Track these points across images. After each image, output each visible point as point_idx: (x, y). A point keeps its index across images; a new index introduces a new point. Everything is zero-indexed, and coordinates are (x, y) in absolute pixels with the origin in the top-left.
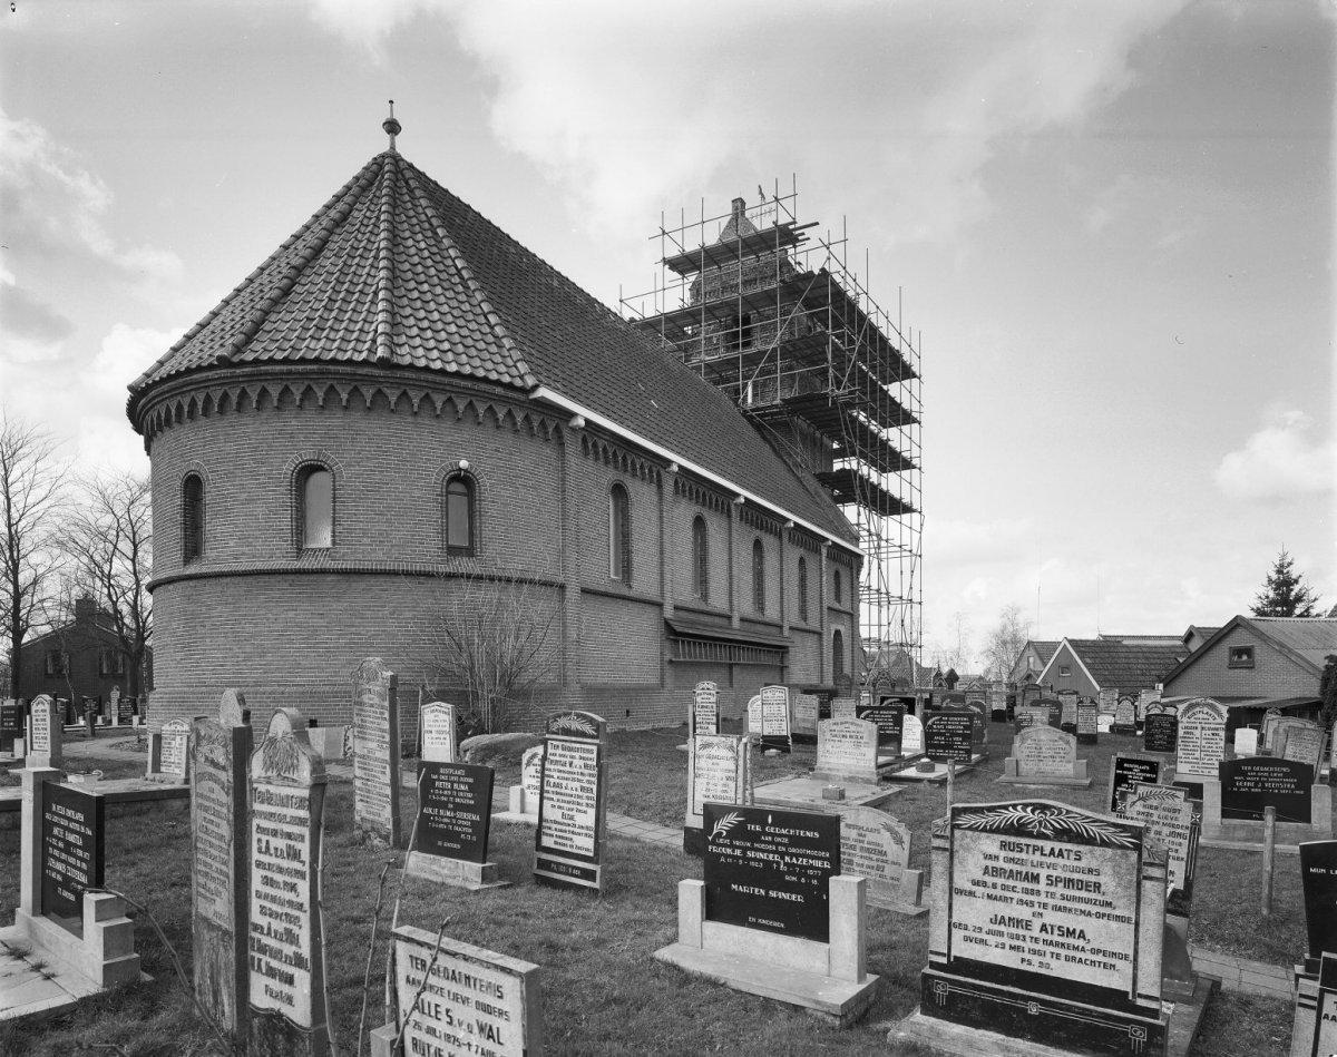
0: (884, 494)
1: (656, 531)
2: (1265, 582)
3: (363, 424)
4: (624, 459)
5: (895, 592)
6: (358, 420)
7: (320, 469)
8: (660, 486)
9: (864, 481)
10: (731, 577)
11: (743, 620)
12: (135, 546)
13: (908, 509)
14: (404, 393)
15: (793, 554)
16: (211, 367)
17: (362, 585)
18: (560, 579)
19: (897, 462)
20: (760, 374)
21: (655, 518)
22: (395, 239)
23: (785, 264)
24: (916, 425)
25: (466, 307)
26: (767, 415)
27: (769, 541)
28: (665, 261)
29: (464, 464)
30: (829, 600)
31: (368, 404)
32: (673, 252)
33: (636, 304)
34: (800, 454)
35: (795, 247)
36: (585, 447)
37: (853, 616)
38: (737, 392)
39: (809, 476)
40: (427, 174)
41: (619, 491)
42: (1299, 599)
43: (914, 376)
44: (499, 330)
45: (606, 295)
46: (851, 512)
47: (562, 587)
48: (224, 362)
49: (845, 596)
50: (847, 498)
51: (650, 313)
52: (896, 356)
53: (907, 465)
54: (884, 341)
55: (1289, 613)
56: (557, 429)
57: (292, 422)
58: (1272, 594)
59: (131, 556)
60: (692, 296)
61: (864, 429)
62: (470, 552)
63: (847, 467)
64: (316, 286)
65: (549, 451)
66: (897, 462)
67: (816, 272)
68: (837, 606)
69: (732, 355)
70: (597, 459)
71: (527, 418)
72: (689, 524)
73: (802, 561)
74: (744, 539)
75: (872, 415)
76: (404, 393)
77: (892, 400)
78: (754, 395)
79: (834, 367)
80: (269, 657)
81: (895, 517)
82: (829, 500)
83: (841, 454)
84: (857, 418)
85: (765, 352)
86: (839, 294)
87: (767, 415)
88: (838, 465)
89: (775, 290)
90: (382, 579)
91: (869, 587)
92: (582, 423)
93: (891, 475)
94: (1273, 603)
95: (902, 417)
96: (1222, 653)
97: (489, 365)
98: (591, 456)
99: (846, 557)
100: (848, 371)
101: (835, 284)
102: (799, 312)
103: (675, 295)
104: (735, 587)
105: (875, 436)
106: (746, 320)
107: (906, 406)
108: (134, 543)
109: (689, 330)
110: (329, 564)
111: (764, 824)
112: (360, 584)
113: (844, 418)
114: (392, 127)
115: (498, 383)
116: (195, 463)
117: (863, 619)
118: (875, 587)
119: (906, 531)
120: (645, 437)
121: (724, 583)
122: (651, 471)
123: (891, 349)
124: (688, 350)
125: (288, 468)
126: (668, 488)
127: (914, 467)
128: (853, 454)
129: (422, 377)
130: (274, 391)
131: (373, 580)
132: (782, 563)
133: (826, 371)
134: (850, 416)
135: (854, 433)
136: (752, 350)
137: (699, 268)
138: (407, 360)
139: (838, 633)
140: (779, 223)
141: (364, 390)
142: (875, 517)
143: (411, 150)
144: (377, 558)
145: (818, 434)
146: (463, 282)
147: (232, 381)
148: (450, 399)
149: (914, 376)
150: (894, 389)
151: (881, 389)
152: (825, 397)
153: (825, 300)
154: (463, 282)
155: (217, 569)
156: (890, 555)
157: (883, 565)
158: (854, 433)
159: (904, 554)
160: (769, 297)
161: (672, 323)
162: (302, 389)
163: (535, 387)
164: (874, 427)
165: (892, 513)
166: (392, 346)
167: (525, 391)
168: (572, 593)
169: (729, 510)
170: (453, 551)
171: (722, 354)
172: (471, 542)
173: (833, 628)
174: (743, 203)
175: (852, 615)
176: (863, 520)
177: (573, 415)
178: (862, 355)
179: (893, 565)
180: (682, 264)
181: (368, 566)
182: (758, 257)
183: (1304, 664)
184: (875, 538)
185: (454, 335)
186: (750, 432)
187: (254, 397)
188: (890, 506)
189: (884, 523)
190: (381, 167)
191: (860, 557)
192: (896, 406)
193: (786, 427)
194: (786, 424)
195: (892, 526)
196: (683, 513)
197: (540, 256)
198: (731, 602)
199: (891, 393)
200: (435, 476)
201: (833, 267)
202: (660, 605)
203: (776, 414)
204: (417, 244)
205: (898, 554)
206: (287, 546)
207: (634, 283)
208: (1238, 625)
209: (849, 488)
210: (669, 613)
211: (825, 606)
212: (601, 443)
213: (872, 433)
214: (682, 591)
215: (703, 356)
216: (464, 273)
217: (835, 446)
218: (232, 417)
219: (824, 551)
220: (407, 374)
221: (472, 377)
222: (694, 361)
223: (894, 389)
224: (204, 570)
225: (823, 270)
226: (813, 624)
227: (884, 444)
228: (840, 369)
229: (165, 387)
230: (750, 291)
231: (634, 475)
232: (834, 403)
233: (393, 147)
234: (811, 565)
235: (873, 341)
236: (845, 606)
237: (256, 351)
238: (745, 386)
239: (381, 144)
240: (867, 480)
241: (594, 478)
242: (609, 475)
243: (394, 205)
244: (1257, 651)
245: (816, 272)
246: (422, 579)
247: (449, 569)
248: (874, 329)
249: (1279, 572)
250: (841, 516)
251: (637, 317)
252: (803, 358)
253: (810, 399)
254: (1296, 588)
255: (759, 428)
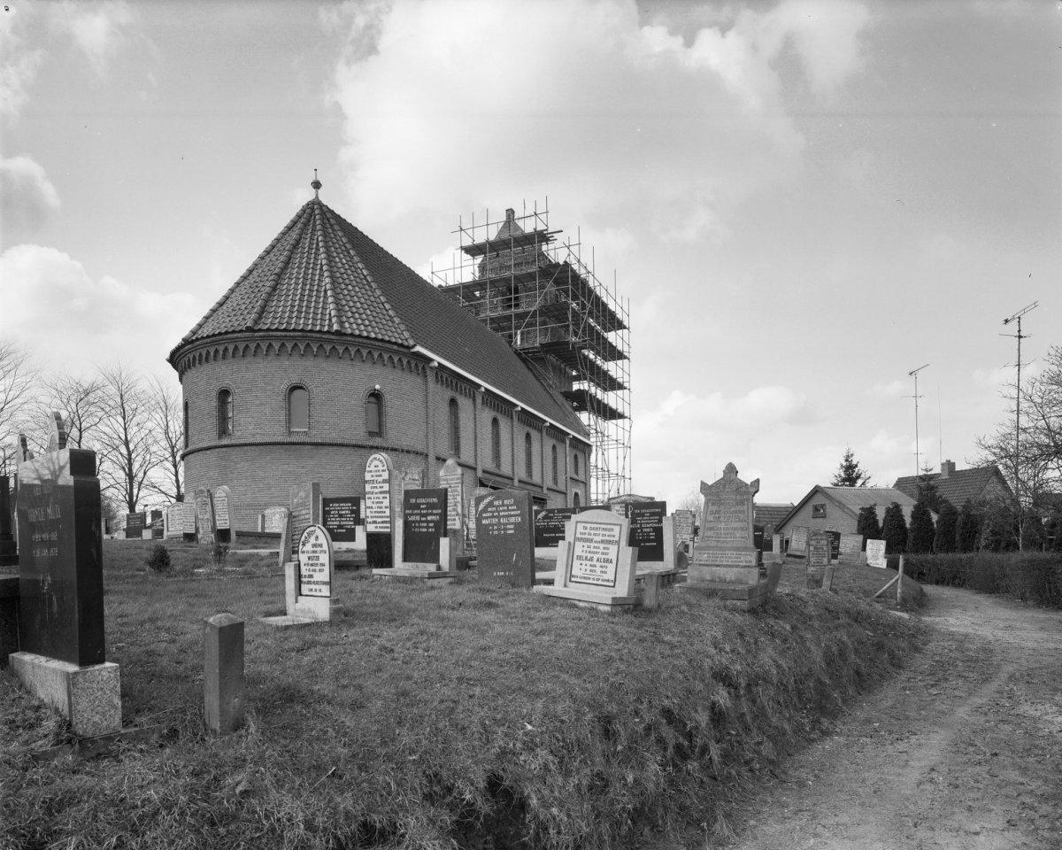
0: (606, 406)
1: (473, 426)
2: (839, 467)
3: (324, 365)
4: (456, 384)
5: (613, 470)
6: (323, 363)
7: (301, 388)
8: (474, 400)
9: (593, 398)
10: (513, 455)
11: (520, 481)
12: (81, 433)
13: (621, 416)
14: (347, 349)
15: (549, 442)
16: (241, 331)
17: (325, 451)
18: (425, 452)
19: (612, 384)
20: (526, 326)
21: (472, 417)
22: (330, 258)
23: (541, 254)
24: (626, 361)
25: (372, 299)
26: (529, 353)
27: (535, 434)
28: (462, 248)
29: (377, 387)
30: (570, 472)
31: (302, 352)
32: (468, 242)
33: (442, 275)
34: (552, 379)
35: (547, 244)
36: (437, 378)
37: (586, 484)
38: (510, 336)
39: (557, 394)
40: (329, 207)
41: (453, 402)
42: (858, 477)
43: (625, 328)
44: (391, 312)
45: (424, 273)
46: (584, 417)
47: (427, 455)
48: (249, 329)
49: (581, 471)
50: (581, 408)
51: (451, 283)
52: (612, 315)
53: (621, 387)
54: (605, 306)
55: (853, 486)
56: (423, 368)
57: (286, 362)
58: (843, 475)
59: (77, 439)
60: (480, 271)
61: (592, 363)
62: (379, 434)
63: (582, 388)
64: (291, 285)
65: (419, 380)
66: (612, 384)
67: (561, 263)
68: (576, 477)
69: (507, 312)
70: (442, 384)
71: (408, 362)
72: (490, 420)
73: (554, 447)
74: (520, 431)
75: (597, 353)
76: (347, 349)
77: (611, 344)
78: (522, 339)
79: (573, 325)
80: (273, 490)
81: (614, 421)
82: (570, 409)
83: (578, 378)
84: (588, 356)
85: (529, 312)
86: (576, 277)
87: (529, 353)
88: (576, 386)
89: (535, 272)
90: (335, 448)
91: (596, 466)
92: (436, 364)
93: (610, 393)
94: (844, 480)
95: (615, 354)
96: (809, 509)
97: (390, 334)
98: (440, 383)
99: (581, 446)
100: (582, 326)
101: (573, 271)
102: (551, 287)
103: (466, 271)
104: (515, 462)
105: (599, 368)
106: (517, 291)
107: (619, 348)
108: (80, 430)
109: (477, 294)
110: (307, 440)
111: (554, 513)
112: (324, 450)
113: (580, 358)
114: (317, 185)
115: (395, 343)
116: (226, 383)
117: (593, 489)
118: (600, 466)
119: (620, 430)
120: (466, 371)
121: (510, 459)
122: (470, 391)
123: (610, 311)
124: (477, 309)
125: (284, 387)
126: (479, 401)
127: (625, 388)
128: (586, 379)
129: (357, 340)
130: (276, 345)
131: (330, 448)
132: (542, 447)
133: (568, 326)
134: (584, 355)
135: (586, 366)
136: (520, 310)
137: (485, 253)
138: (349, 331)
139: (576, 494)
140: (538, 229)
141: (325, 346)
142: (600, 421)
143: (326, 198)
144: (333, 436)
145: (563, 366)
146: (369, 283)
147: (253, 339)
148: (358, 350)
149: (625, 328)
150: (612, 337)
151: (603, 337)
152: (567, 343)
153: (567, 279)
154: (369, 283)
155: (242, 441)
156: (610, 447)
157: (606, 453)
158: (586, 366)
159: (620, 446)
160: (531, 276)
161: (467, 289)
162: (279, 345)
163: (414, 346)
164: (599, 362)
165: (610, 419)
166: (341, 323)
167: (408, 347)
168: (432, 459)
169: (512, 415)
170: (371, 434)
171: (500, 312)
172: (380, 425)
173: (574, 490)
174: (513, 212)
175: (585, 484)
176: (592, 423)
177: (431, 360)
178: (591, 314)
179: (612, 454)
180: (472, 250)
181: (328, 441)
182: (523, 249)
183: (850, 513)
184: (600, 434)
185: (373, 317)
186: (519, 363)
187: (264, 348)
188: (610, 414)
189: (606, 425)
190: (313, 210)
191: (590, 446)
192: (613, 348)
193: (541, 360)
194: (542, 359)
195: (611, 427)
196: (486, 415)
197: (390, 252)
198: (513, 470)
199: (610, 340)
200: (362, 393)
201: (572, 261)
202: (475, 469)
203: (537, 352)
204: (341, 261)
205: (615, 446)
206: (283, 430)
207: (447, 267)
208: (817, 491)
209: (583, 401)
210: (480, 474)
211: (568, 475)
212: (445, 376)
213: (597, 366)
214: (486, 462)
215: (488, 313)
216: (368, 278)
217: (574, 373)
218: (249, 359)
219: (568, 442)
220: (349, 339)
221: (382, 340)
222: (482, 315)
223: (612, 337)
224: (233, 442)
225: (565, 262)
226: (561, 487)
227: (605, 373)
228: (577, 324)
229: (209, 340)
230: (518, 273)
231: (461, 394)
232: (573, 347)
233: (317, 197)
234: (560, 449)
235: (598, 305)
236: (581, 477)
237: (267, 323)
238: (516, 334)
239: (307, 195)
240: (595, 397)
241: (440, 394)
242: (449, 394)
243: (325, 237)
244: (828, 507)
245: (561, 263)
246: (356, 449)
247: (371, 444)
248: (598, 298)
249: (847, 460)
250: (578, 420)
251: (444, 284)
252: (553, 316)
253: (557, 344)
254: (856, 470)
255: (524, 361)
